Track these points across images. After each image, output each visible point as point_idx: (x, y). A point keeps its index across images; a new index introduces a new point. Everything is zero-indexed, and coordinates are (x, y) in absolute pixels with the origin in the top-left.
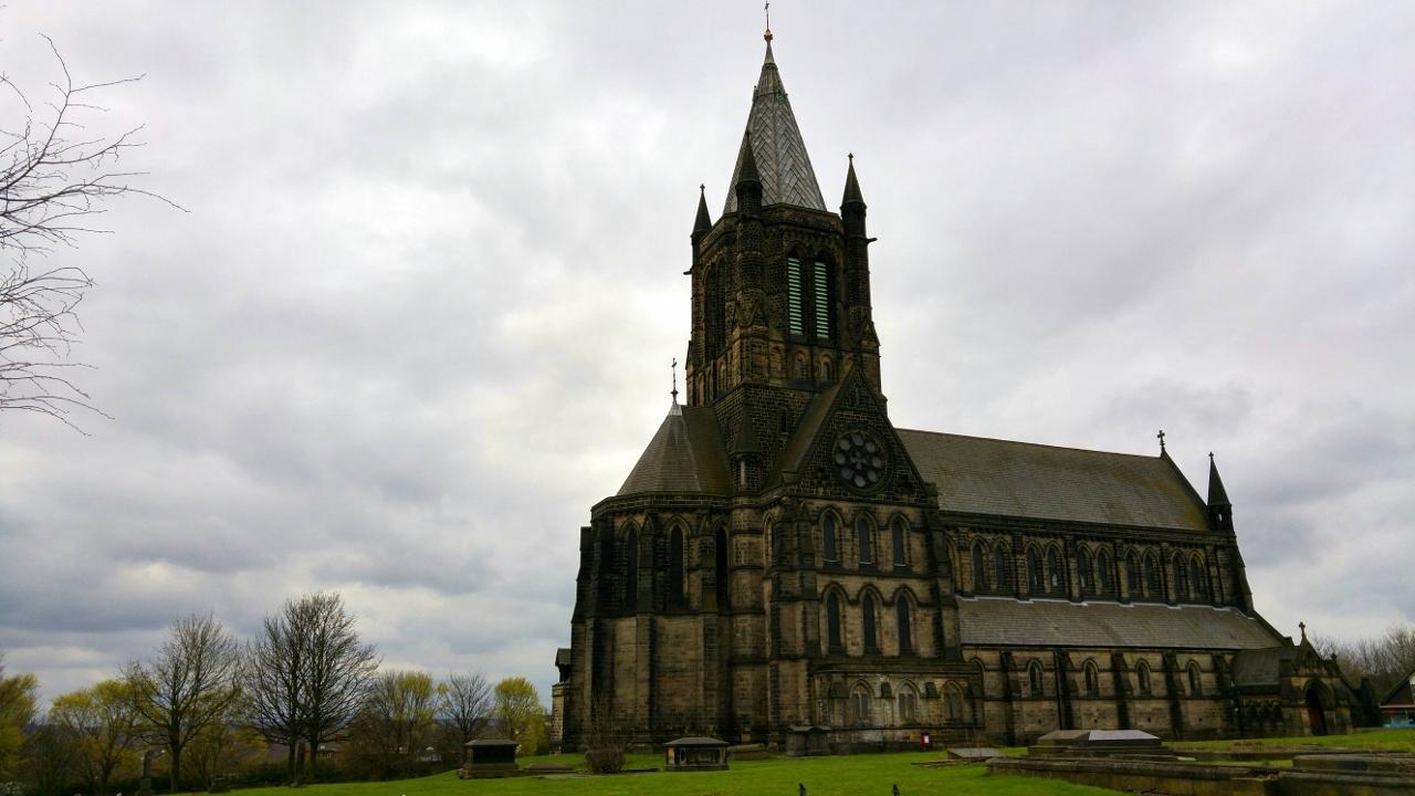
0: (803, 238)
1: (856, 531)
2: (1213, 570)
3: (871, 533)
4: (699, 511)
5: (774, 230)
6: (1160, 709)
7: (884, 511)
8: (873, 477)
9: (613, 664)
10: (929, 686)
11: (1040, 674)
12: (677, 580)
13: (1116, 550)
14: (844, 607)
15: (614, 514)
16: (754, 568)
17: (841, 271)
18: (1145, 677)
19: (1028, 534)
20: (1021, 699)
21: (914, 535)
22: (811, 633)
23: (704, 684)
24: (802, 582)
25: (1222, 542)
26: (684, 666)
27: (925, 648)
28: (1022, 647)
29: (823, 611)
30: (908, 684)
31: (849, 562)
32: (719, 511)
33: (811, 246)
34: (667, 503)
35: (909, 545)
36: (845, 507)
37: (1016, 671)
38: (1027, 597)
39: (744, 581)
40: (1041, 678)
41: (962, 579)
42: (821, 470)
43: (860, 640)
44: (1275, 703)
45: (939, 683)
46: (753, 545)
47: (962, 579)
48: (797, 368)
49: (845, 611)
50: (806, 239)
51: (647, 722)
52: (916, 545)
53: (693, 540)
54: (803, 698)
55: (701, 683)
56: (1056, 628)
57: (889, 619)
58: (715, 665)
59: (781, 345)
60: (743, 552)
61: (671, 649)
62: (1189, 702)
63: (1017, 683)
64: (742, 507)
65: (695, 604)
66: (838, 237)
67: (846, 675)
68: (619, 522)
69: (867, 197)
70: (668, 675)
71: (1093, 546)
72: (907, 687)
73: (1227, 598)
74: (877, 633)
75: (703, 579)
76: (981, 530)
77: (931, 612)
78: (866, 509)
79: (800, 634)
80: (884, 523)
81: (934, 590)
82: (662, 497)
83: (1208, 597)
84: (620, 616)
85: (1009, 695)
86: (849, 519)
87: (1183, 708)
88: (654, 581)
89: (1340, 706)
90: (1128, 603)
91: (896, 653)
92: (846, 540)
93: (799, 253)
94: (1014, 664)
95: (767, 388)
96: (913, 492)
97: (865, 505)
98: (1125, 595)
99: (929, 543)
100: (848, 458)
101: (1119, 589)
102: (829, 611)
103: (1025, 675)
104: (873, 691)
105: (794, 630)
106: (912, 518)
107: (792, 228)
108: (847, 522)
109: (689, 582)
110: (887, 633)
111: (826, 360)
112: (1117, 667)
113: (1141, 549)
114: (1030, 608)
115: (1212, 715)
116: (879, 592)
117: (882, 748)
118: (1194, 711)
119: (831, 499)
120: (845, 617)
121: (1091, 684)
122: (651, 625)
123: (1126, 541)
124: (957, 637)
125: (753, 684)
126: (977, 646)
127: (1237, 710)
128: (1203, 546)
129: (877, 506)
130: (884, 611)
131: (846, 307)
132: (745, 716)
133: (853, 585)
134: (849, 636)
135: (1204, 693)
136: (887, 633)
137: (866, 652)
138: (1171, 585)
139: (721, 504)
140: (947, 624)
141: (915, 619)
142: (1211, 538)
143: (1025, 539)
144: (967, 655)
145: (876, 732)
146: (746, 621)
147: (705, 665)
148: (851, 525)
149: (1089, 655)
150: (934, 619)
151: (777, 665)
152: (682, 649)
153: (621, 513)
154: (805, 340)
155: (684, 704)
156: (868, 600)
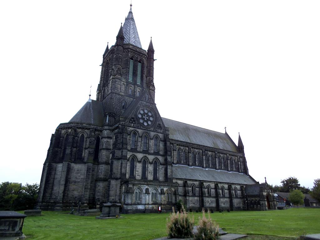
0: (135, 54)
1: (143, 139)
2: (239, 163)
3: (147, 140)
4: (91, 130)
5: (126, 50)
6: (227, 201)
7: (152, 134)
8: (149, 123)
9: (54, 179)
10: (162, 190)
11: (195, 188)
12: (80, 151)
13: (215, 155)
14: (136, 163)
15: (62, 128)
16: (107, 149)
17: (146, 67)
18: (223, 191)
19: (193, 148)
20: (189, 196)
21: (161, 142)
22: (123, 171)
23: (85, 187)
24: (122, 153)
25: (242, 155)
26: (79, 180)
27: (161, 178)
28: (190, 180)
29: (129, 164)
30: (155, 189)
31: (139, 148)
32: (98, 130)
33: (137, 57)
34: (80, 126)
35: (159, 145)
36: (140, 131)
37: (188, 187)
38: (191, 166)
39: (104, 153)
40: (195, 190)
41: (173, 159)
42: (133, 118)
43: (140, 174)
44: (258, 200)
45: (165, 189)
46: (107, 142)
47: (173, 159)
48: (130, 91)
49: (136, 164)
50: (136, 55)
51: (62, 199)
52: (161, 145)
53: (87, 139)
54: (118, 193)
55: (84, 186)
56: (200, 175)
57: (150, 168)
58: (90, 181)
59: (125, 83)
60: (104, 144)
61: (75, 174)
62: (221, 198)
63: (188, 191)
64: (106, 130)
65: (85, 160)
66: (146, 56)
67: (134, 185)
68: (63, 132)
69: (155, 48)
70: (73, 183)
71: (210, 153)
72: (155, 190)
73: (242, 171)
74: (146, 173)
75: (89, 152)
76: (180, 145)
77: (164, 166)
78: (147, 132)
79: (119, 171)
80: (152, 137)
81: (166, 160)
82: (78, 124)
83: (238, 170)
84: (59, 162)
85: (185, 195)
86: (141, 135)
87: (233, 201)
88: (71, 151)
89: (274, 201)
90: (218, 170)
91: (152, 179)
92: (139, 141)
93: (134, 59)
94: (188, 185)
95: (119, 95)
96: (162, 129)
97: (146, 131)
98: (217, 168)
99: (165, 145)
100: (142, 116)
101: (216, 166)
102: (131, 164)
103: (190, 189)
104: (143, 191)
105: (118, 169)
106: (161, 137)
107: (134, 52)
108: (140, 136)
109: (85, 152)
110: (150, 172)
111: (139, 90)
112: (216, 187)
113: (222, 155)
114: (192, 169)
115: (240, 203)
116: (148, 159)
117: (144, 212)
118: (236, 201)
119: (136, 128)
120: (136, 166)
121: (209, 193)
122: (68, 166)
123: (218, 153)
124: (172, 175)
125: (103, 188)
126: (177, 179)
127: (246, 201)
128: (237, 156)
129: (151, 132)
130: (149, 165)
131: (146, 77)
132: (98, 199)
133: (140, 156)
134: (137, 172)
135: (238, 197)
136: (150, 172)
137: (142, 178)
138: (229, 166)
139: (99, 128)
140: (169, 171)
141: (159, 169)
142: (239, 154)
143: (192, 149)
144: (174, 181)
145: (143, 205)
146: (102, 166)
147: (86, 180)
148: (141, 137)
149: (209, 184)
150: (165, 169)
151: (110, 181)
152: (79, 175)
153: (64, 128)
154: (133, 83)
155: (77, 194)
156: (145, 162)
